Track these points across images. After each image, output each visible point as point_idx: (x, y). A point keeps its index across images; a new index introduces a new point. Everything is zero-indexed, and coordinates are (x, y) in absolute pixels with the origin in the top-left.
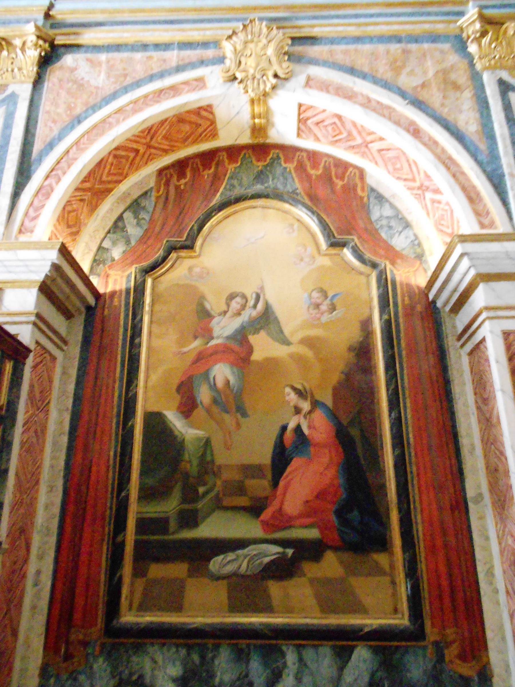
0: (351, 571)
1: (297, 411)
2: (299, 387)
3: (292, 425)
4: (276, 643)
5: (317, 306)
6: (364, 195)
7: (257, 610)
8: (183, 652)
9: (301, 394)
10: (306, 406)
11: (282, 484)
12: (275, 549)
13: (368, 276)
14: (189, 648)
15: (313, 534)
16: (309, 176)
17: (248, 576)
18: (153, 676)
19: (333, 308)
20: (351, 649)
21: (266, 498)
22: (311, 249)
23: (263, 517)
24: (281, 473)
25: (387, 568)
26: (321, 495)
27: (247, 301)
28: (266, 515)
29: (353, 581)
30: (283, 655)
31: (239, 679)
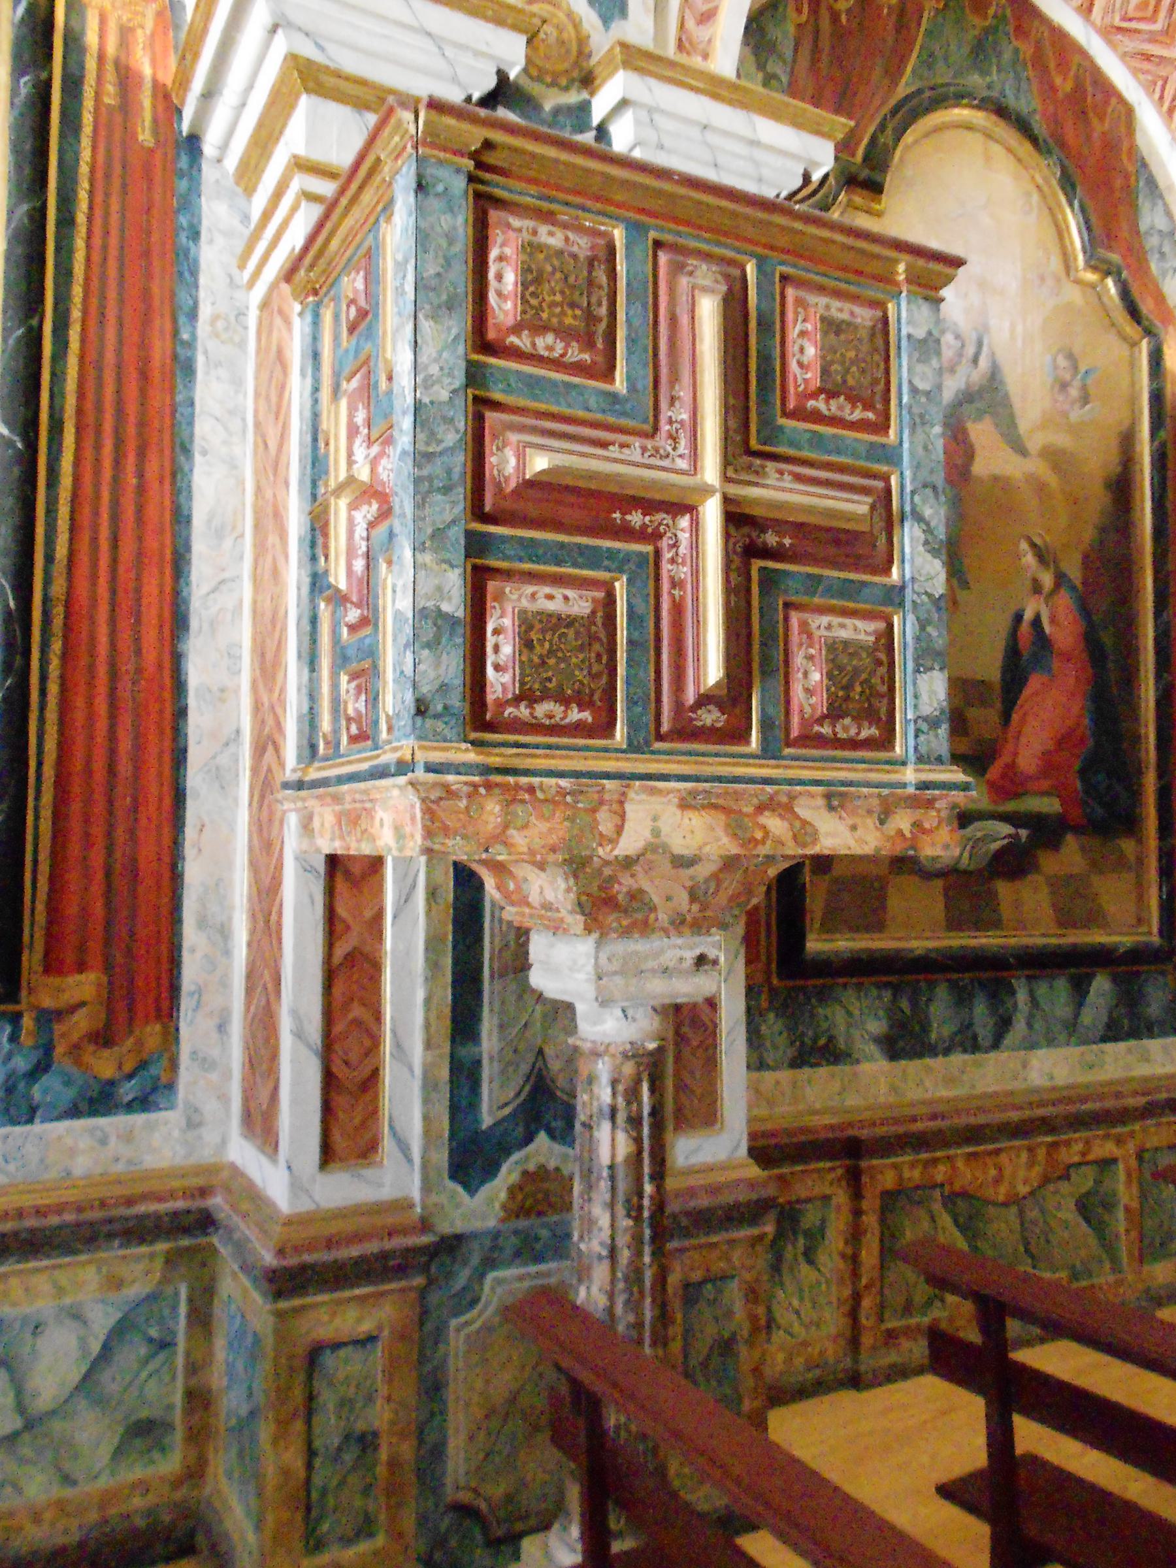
0: (1095, 866)
1: (1037, 588)
2: (1038, 541)
3: (1028, 615)
4: (896, 284)
5: (1064, 386)
6: (1131, 168)
7: (980, 925)
8: (887, 995)
9: (1042, 556)
10: (1047, 580)
11: (1015, 717)
12: (1006, 829)
13: (1134, 344)
14: (897, 990)
15: (1049, 805)
16: (1053, 89)
17: (971, 873)
18: (849, 1037)
19: (1085, 399)
20: (1090, 977)
21: (995, 741)
22: (1056, 263)
23: (988, 776)
24: (1014, 703)
25: (1132, 858)
26: (1062, 741)
27: (963, 346)
28: (994, 772)
29: (1095, 879)
30: (1013, 993)
31: (960, 1031)
